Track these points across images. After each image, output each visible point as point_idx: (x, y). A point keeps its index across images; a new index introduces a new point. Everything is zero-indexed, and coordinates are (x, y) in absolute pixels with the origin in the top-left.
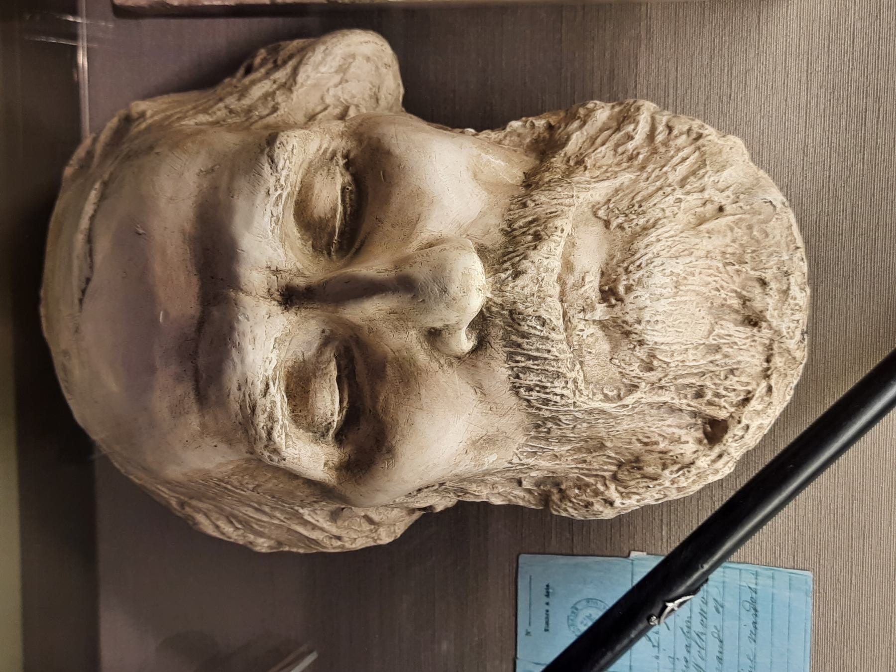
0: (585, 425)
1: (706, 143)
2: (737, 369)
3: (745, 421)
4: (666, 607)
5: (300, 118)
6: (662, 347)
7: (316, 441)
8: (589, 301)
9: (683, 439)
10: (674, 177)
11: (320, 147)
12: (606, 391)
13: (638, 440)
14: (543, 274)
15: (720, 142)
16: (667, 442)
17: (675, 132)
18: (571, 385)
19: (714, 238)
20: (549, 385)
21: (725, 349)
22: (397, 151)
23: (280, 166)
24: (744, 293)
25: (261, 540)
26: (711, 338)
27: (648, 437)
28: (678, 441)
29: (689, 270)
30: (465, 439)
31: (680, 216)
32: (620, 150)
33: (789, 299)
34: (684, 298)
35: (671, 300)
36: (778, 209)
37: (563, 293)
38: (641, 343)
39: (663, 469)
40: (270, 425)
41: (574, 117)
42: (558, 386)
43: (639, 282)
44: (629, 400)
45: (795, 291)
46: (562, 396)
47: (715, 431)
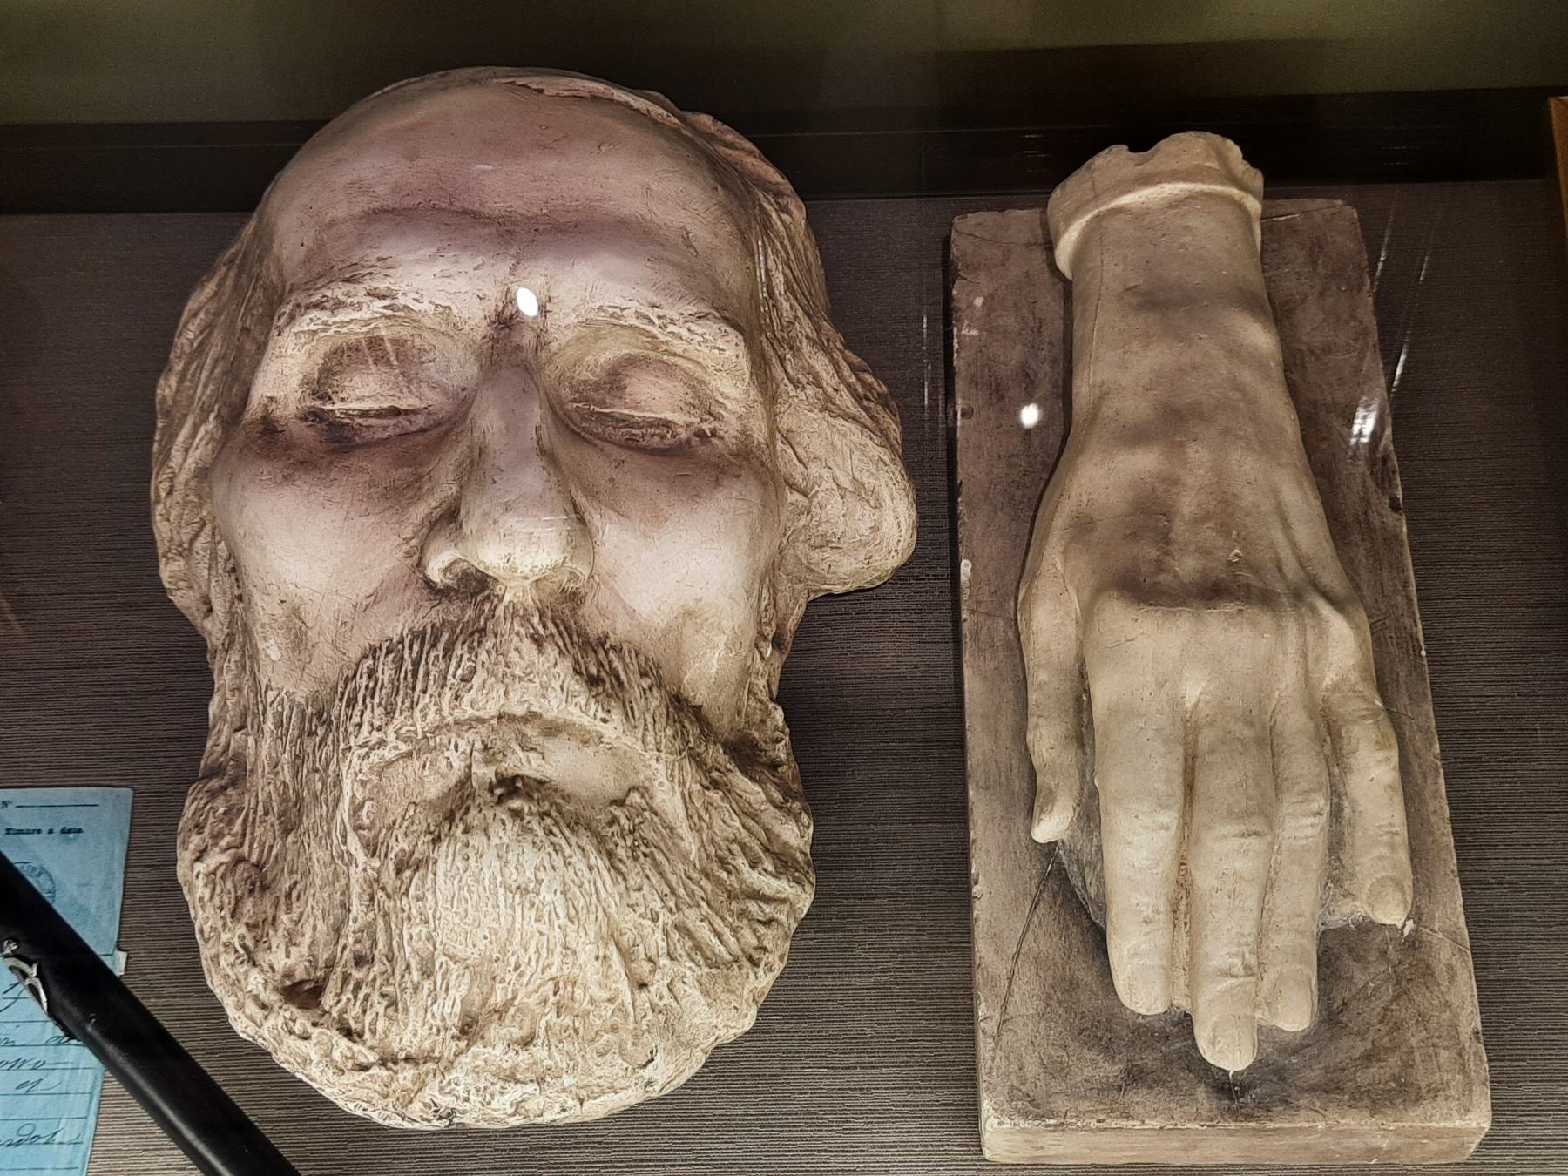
0: (319, 786)
1: (744, 971)
2: (396, 1010)
3: (315, 1032)
4: (31, 965)
5: (785, 422)
6: (430, 876)
7: (305, 382)
8: (500, 757)
9: (293, 949)
10: (691, 917)
11: (727, 398)
12: (368, 804)
13: (295, 883)
14: (537, 681)
15: (746, 991)
16: (289, 925)
17: (762, 929)
18: (376, 735)
19: (597, 964)
20: (377, 700)
21: (427, 984)
22: (720, 495)
23: (693, 327)
24: (512, 1010)
25: (173, 381)
26: (444, 959)
27: (298, 898)
28: (291, 942)
29: (545, 912)
30: (300, 592)
31: (632, 916)
32: (735, 847)
33: (501, 1083)
34: (501, 898)
35: (499, 879)
36: (641, 1072)
37: (513, 718)
38: (436, 841)
39: (247, 925)
40: (328, 305)
41: (787, 793)
42: (374, 715)
43: (527, 830)
44: (354, 844)
45: (515, 1092)
46: (360, 725)
47: (303, 993)
